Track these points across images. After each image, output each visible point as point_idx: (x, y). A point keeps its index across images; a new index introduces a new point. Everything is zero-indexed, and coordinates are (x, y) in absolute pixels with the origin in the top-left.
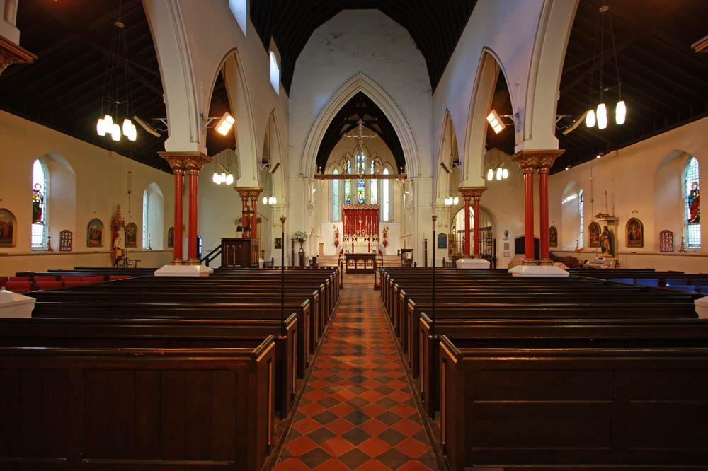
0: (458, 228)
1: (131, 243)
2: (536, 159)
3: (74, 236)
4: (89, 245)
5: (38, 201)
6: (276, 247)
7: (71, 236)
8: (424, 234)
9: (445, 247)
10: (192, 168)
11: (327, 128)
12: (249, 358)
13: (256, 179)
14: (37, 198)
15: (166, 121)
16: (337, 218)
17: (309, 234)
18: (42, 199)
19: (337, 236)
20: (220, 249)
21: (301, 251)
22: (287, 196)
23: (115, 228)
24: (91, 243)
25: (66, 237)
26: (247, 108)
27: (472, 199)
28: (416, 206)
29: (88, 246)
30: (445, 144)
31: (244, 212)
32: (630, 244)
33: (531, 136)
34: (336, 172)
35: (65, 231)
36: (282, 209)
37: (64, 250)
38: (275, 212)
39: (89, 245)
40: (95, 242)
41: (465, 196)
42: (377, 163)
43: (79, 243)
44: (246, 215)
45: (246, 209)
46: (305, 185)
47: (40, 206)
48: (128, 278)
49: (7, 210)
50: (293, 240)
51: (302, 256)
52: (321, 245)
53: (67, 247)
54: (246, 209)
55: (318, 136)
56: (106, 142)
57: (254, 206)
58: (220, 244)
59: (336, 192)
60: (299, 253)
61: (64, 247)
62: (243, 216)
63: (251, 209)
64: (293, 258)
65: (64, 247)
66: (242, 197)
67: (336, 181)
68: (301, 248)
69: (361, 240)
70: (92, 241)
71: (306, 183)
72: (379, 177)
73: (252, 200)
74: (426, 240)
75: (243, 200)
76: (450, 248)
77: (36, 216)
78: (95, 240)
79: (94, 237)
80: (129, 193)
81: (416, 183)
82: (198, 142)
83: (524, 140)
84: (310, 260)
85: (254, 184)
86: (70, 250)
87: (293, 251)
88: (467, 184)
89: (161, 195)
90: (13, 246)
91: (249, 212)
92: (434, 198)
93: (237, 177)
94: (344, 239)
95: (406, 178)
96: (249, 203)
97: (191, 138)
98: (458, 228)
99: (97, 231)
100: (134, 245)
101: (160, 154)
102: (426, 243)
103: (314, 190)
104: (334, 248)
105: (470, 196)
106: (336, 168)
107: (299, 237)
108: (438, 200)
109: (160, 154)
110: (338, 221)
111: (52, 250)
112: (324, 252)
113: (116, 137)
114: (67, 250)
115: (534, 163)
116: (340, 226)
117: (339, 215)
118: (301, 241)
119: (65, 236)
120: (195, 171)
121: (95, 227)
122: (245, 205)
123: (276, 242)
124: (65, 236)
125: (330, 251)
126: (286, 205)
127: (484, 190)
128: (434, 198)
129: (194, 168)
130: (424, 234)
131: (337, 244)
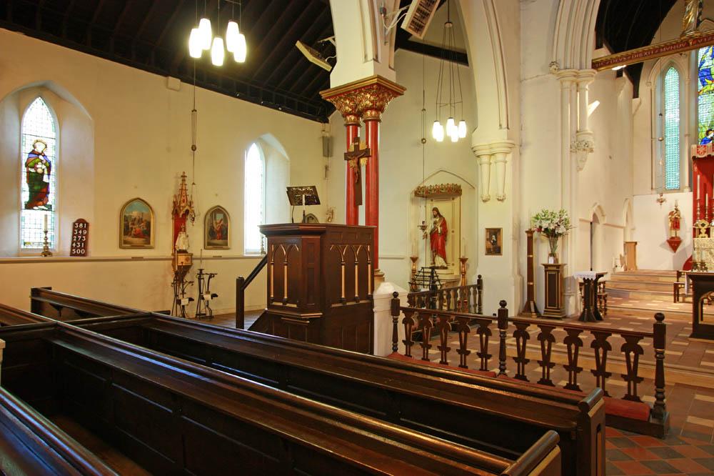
1: (216, 241)
3: (91, 228)
4: (124, 244)
5: (40, 171)
7: (87, 229)
10: (367, 108)
12: (576, 408)
14: (39, 165)
15: (334, 39)
16: (672, 181)
18: (49, 168)
19: (676, 224)
21: (551, 261)
22: (514, 123)
23: (181, 218)
24: (126, 242)
25: (81, 230)
26: (488, 15)
29: (121, 247)
32: (209, 245)
35: (80, 221)
36: (500, 157)
37: (76, 255)
38: (485, 167)
39: (124, 244)
40: (220, 242)
43: (104, 241)
46: (562, 89)
47: (45, 179)
48: (53, 328)
49: (143, 201)
50: (530, 232)
51: (555, 275)
52: (631, 246)
53: (81, 248)
56: (201, 75)
59: (672, 116)
60: (546, 266)
61: (76, 248)
64: (530, 278)
65: (76, 248)
68: (552, 255)
69: (191, 311)
70: (129, 238)
71: (567, 84)
77: (39, 196)
78: (136, 236)
79: (135, 230)
80: (194, 148)
82: (508, 128)
84: (581, 284)
86: (84, 255)
87: (530, 261)
89: (287, 157)
90: (228, 249)
93: (473, 127)
94: (696, 233)
97: (366, 56)
99: (140, 221)
100: (224, 246)
101: (324, 94)
103: (592, 107)
104: (669, 253)
106: (671, 65)
107: (545, 225)
109: (324, 94)
110: (679, 190)
111: (50, 254)
112: (638, 264)
113: (218, 61)
114: (80, 255)
116: (685, 202)
117: (681, 171)
119: (79, 229)
120: (374, 113)
121: (135, 214)
124: (79, 229)
125: (656, 259)
126: (512, 146)
129: (371, 109)
131: (674, 244)
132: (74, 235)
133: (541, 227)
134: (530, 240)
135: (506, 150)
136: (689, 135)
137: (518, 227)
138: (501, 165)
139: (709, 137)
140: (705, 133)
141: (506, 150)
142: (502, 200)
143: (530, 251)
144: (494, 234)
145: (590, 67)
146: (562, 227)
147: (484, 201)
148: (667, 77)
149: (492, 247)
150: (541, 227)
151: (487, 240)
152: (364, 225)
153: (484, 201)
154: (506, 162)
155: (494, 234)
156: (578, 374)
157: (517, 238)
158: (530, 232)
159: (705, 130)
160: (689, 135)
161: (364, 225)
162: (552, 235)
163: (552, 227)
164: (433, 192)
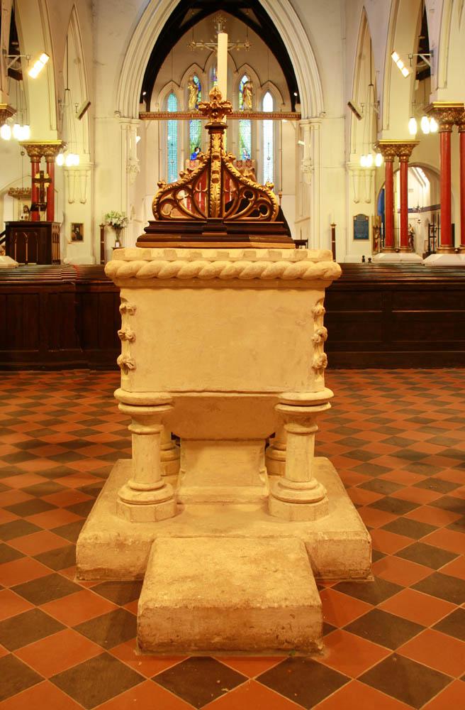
0: (132, 225)
2: (453, 114)
6: (356, 238)
8: (330, 216)
9: (367, 238)
11: (163, 25)
13: (87, 152)
17: (129, 216)
20: (4, 236)
27: (397, 158)
28: (316, 166)
30: (362, 62)
31: (34, 180)
33: (446, 83)
34: (172, 107)
41: (385, 155)
42: (248, 91)
44: (38, 185)
45: (38, 176)
50: (102, 226)
54: (38, 176)
55: (145, 44)
57: (51, 170)
58: (4, 229)
62: (33, 185)
63: (46, 176)
66: (32, 156)
67: (173, 124)
68: (118, 241)
72: (255, 116)
73: (47, 162)
74: (334, 225)
75: (32, 162)
76: (374, 239)
81: (316, 127)
83: (437, 88)
85: (51, 138)
87: (102, 246)
88: (388, 137)
91: (42, 180)
92: (347, 153)
95: (299, 117)
96: (43, 166)
97: (84, 151)
98: (132, 225)
102: (333, 231)
105: (393, 155)
107: (114, 221)
108: (352, 156)
112: (250, 125)
115: (451, 119)
118: (118, 228)
122: (35, 169)
123: (74, 231)
127: (414, 146)
128: (347, 153)
130: (330, 216)
132: (429, 237)
133: (111, 223)
134: (103, 232)
135: (88, 168)
136: (184, 150)
137: (93, 223)
138: (83, 178)
139: (197, 153)
140: (193, 149)
141: (88, 168)
142: (84, 203)
143: (102, 238)
145: (138, 117)
146: (125, 222)
147: (70, 203)
148: (169, 101)
149: (76, 236)
150: (111, 223)
151: (73, 231)
152: (46, 220)
153: (70, 203)
154: (87, 176)
156: (178, 256)
157: (93, 230)
158: (102, 226)
159: (194, 147)
160: (184, 150)
161: (46, 220)
162: (118, 228)
163: (118, 223)
164: (25, 193)
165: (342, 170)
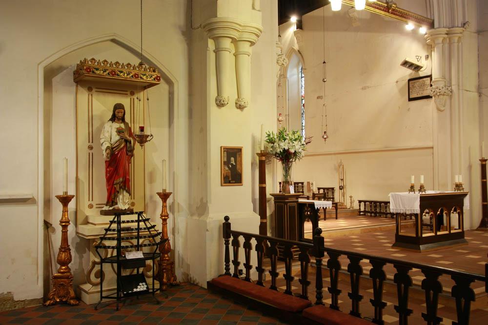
28: (454, 88)
144: (232, 154)
151: (225, 163)
155: (232, 154)
165: (476, 95)
